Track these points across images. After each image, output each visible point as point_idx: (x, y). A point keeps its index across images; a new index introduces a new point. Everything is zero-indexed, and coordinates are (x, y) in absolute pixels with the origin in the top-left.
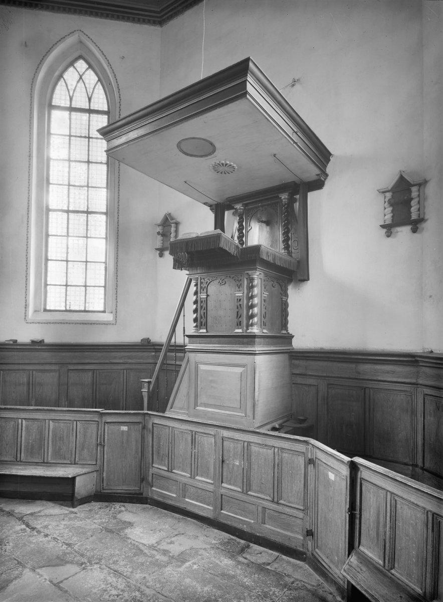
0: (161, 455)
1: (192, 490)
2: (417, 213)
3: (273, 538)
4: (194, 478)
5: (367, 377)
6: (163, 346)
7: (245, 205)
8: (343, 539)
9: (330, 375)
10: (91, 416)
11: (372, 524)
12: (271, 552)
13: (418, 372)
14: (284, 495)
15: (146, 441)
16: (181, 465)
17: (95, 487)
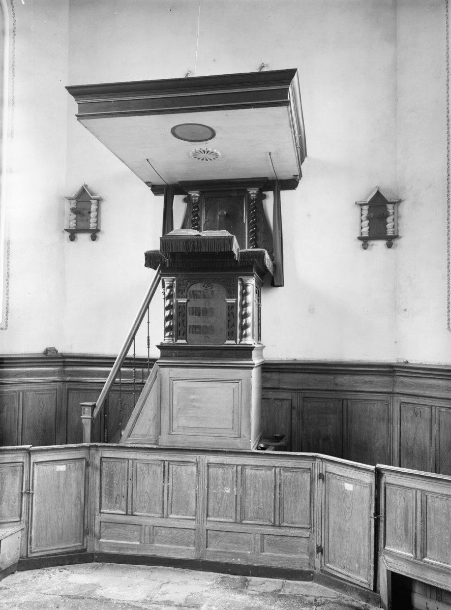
0: (115, 496)
1: (164, 532)
2: (392, 229)
3: (274, 565)
4: (167, 517)
5: (345, 389)
6: (115, 358)
7: (202, 193)
8: (367, 544)
9: (307, 388)
10: (13, 456)
11: (399, 523)
12: (271, 579)
13: (395, 382)
14: (287, 517)
15: (91, 481)
16: (147, 504)
17: (19, 550)
